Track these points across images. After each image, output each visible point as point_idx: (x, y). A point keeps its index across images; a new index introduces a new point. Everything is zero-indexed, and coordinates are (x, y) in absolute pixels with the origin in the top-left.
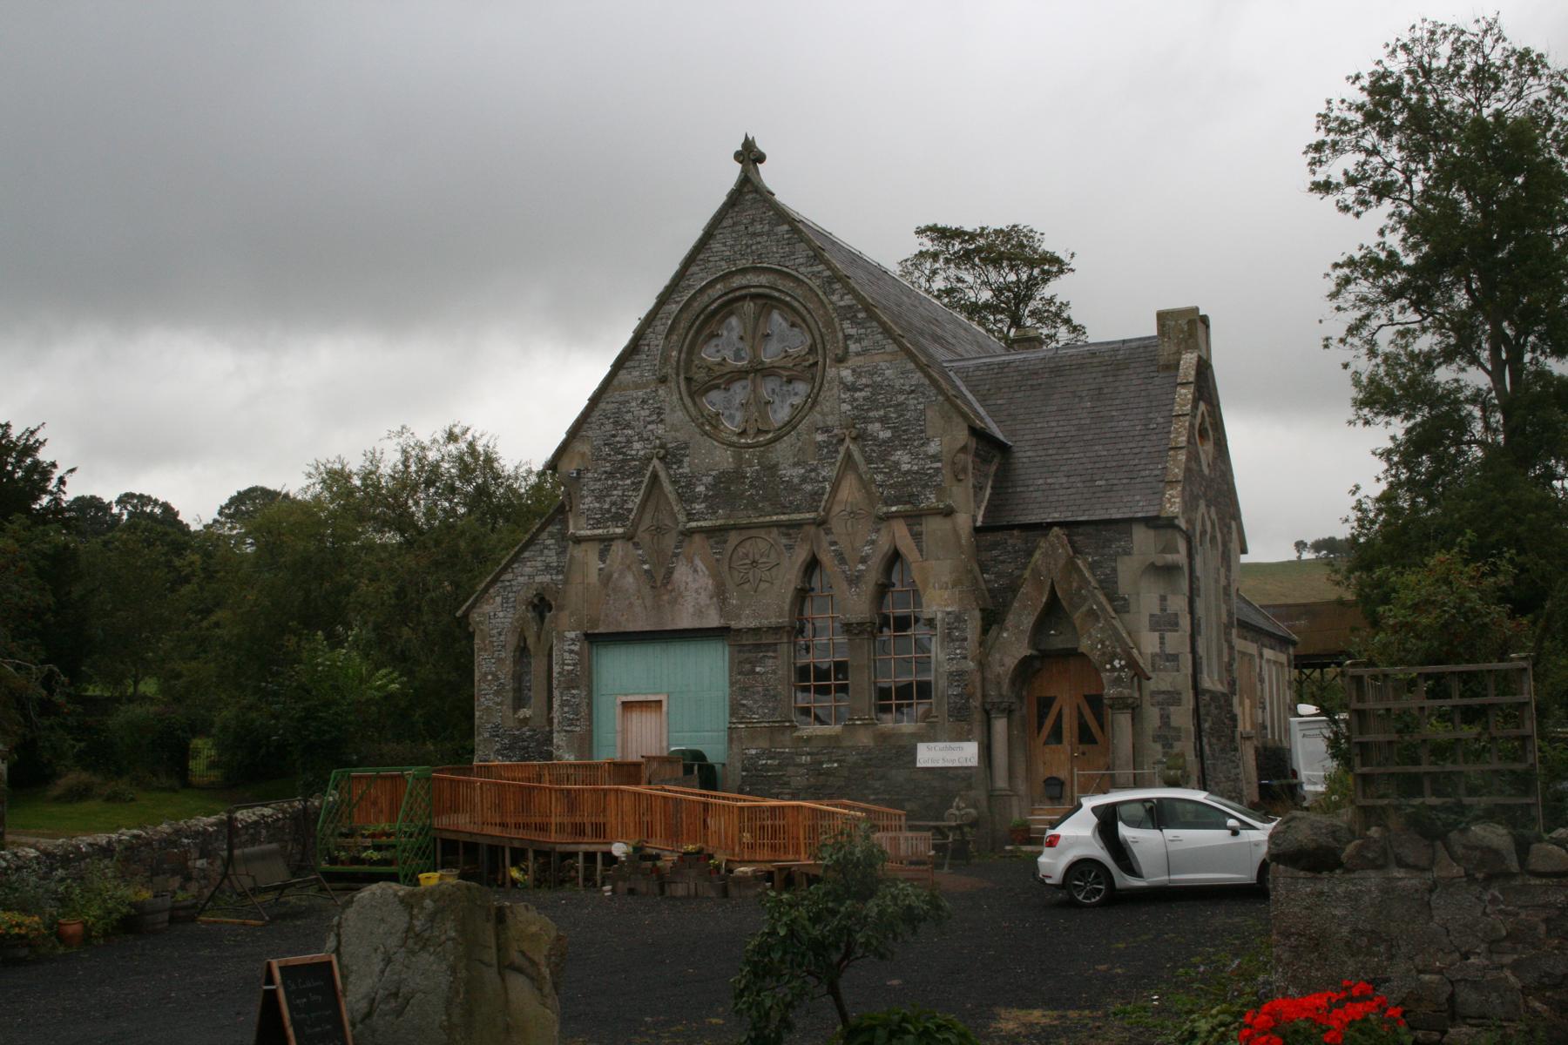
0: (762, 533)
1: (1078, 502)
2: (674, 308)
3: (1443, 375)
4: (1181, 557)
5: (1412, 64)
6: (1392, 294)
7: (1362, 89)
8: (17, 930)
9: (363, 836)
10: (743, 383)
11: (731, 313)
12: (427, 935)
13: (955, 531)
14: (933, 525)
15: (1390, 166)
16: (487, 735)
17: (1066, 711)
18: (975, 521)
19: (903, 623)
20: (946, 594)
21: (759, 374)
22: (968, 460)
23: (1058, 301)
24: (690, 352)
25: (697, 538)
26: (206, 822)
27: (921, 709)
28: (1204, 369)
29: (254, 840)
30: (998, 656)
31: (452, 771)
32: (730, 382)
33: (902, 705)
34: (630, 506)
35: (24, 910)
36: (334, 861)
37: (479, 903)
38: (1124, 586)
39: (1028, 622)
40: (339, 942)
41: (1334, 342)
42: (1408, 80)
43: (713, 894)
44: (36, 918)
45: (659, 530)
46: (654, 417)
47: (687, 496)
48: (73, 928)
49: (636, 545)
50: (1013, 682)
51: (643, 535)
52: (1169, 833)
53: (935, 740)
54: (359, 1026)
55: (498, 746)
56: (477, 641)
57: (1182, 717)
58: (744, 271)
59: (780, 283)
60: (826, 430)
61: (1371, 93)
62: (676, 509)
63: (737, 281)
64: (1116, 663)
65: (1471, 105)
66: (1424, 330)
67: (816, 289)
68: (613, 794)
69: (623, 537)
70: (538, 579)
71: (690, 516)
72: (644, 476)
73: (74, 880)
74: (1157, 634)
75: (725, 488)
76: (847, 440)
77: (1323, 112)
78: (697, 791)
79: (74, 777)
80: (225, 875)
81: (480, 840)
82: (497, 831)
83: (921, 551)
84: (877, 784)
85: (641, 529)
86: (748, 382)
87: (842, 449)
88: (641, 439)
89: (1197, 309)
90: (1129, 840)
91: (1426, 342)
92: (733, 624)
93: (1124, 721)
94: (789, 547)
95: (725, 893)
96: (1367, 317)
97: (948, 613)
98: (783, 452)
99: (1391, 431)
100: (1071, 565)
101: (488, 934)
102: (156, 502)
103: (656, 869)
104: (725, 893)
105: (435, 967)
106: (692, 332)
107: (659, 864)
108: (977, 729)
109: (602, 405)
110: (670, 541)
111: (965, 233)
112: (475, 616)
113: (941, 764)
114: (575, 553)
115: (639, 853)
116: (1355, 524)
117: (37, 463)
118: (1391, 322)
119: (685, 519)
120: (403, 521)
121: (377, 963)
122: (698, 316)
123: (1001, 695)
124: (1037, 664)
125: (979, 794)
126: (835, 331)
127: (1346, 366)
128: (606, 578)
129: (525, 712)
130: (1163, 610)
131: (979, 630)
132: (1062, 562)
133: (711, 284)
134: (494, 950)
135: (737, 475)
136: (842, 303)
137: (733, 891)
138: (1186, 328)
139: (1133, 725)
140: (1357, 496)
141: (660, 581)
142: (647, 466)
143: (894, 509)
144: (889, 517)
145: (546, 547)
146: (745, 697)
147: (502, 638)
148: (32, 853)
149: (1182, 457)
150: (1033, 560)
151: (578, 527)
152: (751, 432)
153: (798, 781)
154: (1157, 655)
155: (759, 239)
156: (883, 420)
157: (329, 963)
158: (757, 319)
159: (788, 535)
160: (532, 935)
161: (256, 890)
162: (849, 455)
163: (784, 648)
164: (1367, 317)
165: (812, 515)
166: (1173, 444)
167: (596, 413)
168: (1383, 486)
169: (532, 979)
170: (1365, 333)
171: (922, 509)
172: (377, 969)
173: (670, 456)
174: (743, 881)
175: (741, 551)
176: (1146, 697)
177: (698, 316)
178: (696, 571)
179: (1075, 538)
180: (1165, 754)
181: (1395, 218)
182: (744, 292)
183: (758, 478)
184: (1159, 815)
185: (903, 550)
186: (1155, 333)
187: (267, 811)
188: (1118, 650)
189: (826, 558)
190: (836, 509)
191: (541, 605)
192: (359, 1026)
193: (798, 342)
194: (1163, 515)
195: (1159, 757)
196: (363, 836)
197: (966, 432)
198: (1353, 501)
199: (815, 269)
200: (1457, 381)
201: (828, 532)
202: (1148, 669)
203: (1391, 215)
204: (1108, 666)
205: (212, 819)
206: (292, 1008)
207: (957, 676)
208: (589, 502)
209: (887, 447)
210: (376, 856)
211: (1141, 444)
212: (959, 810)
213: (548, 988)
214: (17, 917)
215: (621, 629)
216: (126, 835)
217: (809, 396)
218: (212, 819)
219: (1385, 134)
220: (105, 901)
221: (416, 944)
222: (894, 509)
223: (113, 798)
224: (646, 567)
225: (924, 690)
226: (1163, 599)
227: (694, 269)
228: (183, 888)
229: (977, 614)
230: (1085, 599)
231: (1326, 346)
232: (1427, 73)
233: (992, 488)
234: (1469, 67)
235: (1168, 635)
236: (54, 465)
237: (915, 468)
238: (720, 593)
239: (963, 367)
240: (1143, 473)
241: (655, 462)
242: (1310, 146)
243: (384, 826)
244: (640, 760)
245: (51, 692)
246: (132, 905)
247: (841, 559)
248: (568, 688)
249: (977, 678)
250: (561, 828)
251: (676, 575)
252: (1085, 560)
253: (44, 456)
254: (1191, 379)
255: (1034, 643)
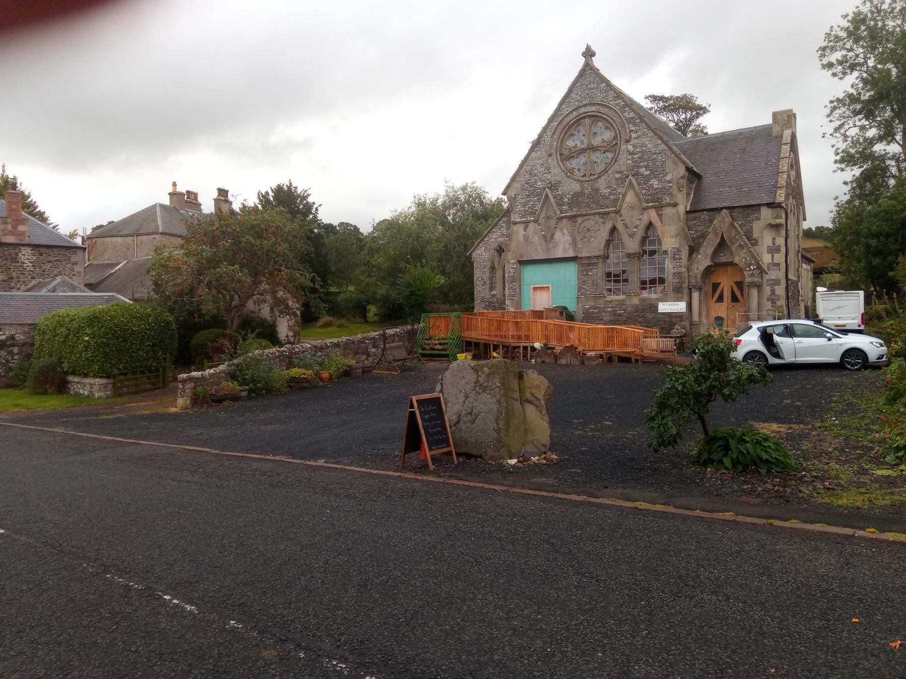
0: (592, 217)
1: (734, 198)
2: (555, 124)
3: (879, 148)
4: (782, 221)
5: (873, 8)
6: (856, 113)
7: (848, 21)
8: (303, 376)
9: (435, 339)
10: (584, 154)
11: (579, 125)
12: (485, 385)
13: (678, 213)
14: (668, 211)
15: (857, 56)
16: (479, 301)
17: (725, 289)
18: (686, 208)
19: (652, 253)
20: (673, 240)
21: (591, 150)
22: (684, 181)
23: (702, 126)
24: (562, 142)
25: (564, 221)
26: (373, 334)
27: (660, 289)
28: (794, 136)
29: (393, 341)
30: (696, 266)
31: (466, 314)
32: (578, 154)
33: (651, 287)
34: (537, 208)
35: (306, 367)
36: (424, 349)
37: (510, 369)
38: (756, 234)
39: (710, 250)
40: (442, 387)
41: (827, 136)
42: (869, 15)
43: (577, 363)
44: (311, 371)
45: (548, 218)
46: (546, 171)
47: (560, 203)
48: (325, 375)
49: (539, 225)
50: (702, 277)
51: (541, 221)
52: (796, 339)
53: (666, 301)
54: (453, 428)
55: (484, 305)
56: (475, 264)
57: (780, 290)
58: (585, 106)
59: (602, 109)
60: (621, 172)
61: (852, 22)
62: (556, 209)
63: (582, 110)
64: (752, 267)
65: (899, 26)
66: (871, 128)
67: (618, 111)
68: (539, 323)
69: (533, 221)
70: (499, 240)
71: (561, 212)
72: (542, 196)
73: (325, 356)
74: (771, 254)
75: (576, 199)
76: (630, 176)
77: (828, 32)
78: (566, 322)
79: (326, 318)
80: (383, 355)
81: (480, 341)
82: (487, 338)
83: (662, 222)
84: (640, 320)
85: (541, 217)
86: (587, 154)
87: (627, 180)
88: (541, 180)
89: (791, 110)
90: (779, 342)
91: (872, 133)
92: (579, 255)
93: (754, 292)
94: (604, 223)
95: (583, 363)
96: (843, 124)
97: (674, 248)
98: (602, 183)
99: (853, 173)
100: (732, 225)
101: (515, 384)
102: (351, 225)
103: (553, 353)
104: (583, 363)
105: (490, 400)
106: (563, 134)
107: (554, 351)
108: (686, 297)
109: (525, 167)
110: (553, 222)
111: (665, 98)
112: (474, 255)
113: (669, 311)
114: (514, 229)
115: (546, 347)
116: (835, 213)
117: (308, 203)
118: (855, 126)
119: (559, 213)
120: (444, 222)
121: (461, 397)
122: (565, 127)
123: (697, 282)
124: (713, 269)
125: (686, 323)
126: (625, 129)
127: (833, 146)
128: (526, 238)
129: (494, 292)
130: (774, 244)
131: (687, 254)
132: (727, 224)
133: (571, 112)
134: (518, 392)
135: (582, 193)
136: (629, 116)
137: (587, 363)
138: (786, 119)
139: (758, 294)
140: (837, 201)
141: (548, 238)
142: (544, 191)
143: (650, 204)
144: (648, 208)
145: (502, 227)
146: (584, 285)
147: (485, 263)
148: (309, 346)
149: (785, 176)
150: (714, 223)
151: (515, 217)
152: (588, 175)
153: (607, 318)
154: (770, 263)
155: (592, 91)
156: (646, 167)
157: (439, 398)
158: (591, 125)
159: (603, 218)
160: (537, 385)
161: (395, 360)
162: (631, 182)
163: (600, 265)
164: (843, 124)
165: (614, 209)
166: (781, 171)
167: (522, 171)
168: (848, 197)
169: (537, 407)
170: (842, 131)
171: (663, 204)
172: (461, 401)
173: (553, 187)
174: (590, 358)
175: (583, 225)
176: (765, 282)
177: (565, 127)
178: (564, 234)
179: (733, 214)
180: (772, 307)
181: (859, 79)
182: (585, 115)
183: (590, 194)
184: (789, 332)
185: (654, 222)
186: (771, 122)
187: (398, 330)
188: (753, 262)
189: (620, 227)
190: (624, 206)
191: (500, 250)
192: (453, 428)
193: (608, 135)
194: (776, 201)
195: (770, 307)
196: (435, 339)
197: (684, 169)
198: (835, 203)
199: (617, 102)
200: (885, 150)
201: (621, 215)
202: (765, 268)
203: (857, 78)
204: (748, 269)
205: (377, 333)
206: (423, 420)
207: (677, 275)
208: (520, 208)
209: (647, 178)
210: (440, 347)
211: (765, 171)
212: (677, 330)
213: (544, 412)
214: (303, 371)
215: (533, 259)
216: (344, 339)
217: (613, 158)
218: (377, 333)
219: (856, 41)
220: (337, 364)
221: (480, 389)
222: (650, 204)
223: (340, 326)
224: (543, 233)
225: (662, 281)
226: (774, 239)
227: (564, 106)
228: (367, 359)
229: (687, 248)
230: (738, 240)
231: (823, 137)
232: (879, 12)
233: (694, 194)
234: (898, 8)
235: (775, 255)
236: (314, 203)
237: (660, 186)
238: (574, 243)
239: (679, 144)
240: (766, 184)
241: (547, 189)
242: (820, 47)
243: (443, 336)
244: (542, 309)
245: (314, 284)
246: (348, 366)
247: (626, 226)
248: (511, 282)
249: (686, 275)
250: (513, 337)
251: (555, 236)
252: (738, 224)
253: (310, 200)
254: (789, 142)
255: (712, 260)
